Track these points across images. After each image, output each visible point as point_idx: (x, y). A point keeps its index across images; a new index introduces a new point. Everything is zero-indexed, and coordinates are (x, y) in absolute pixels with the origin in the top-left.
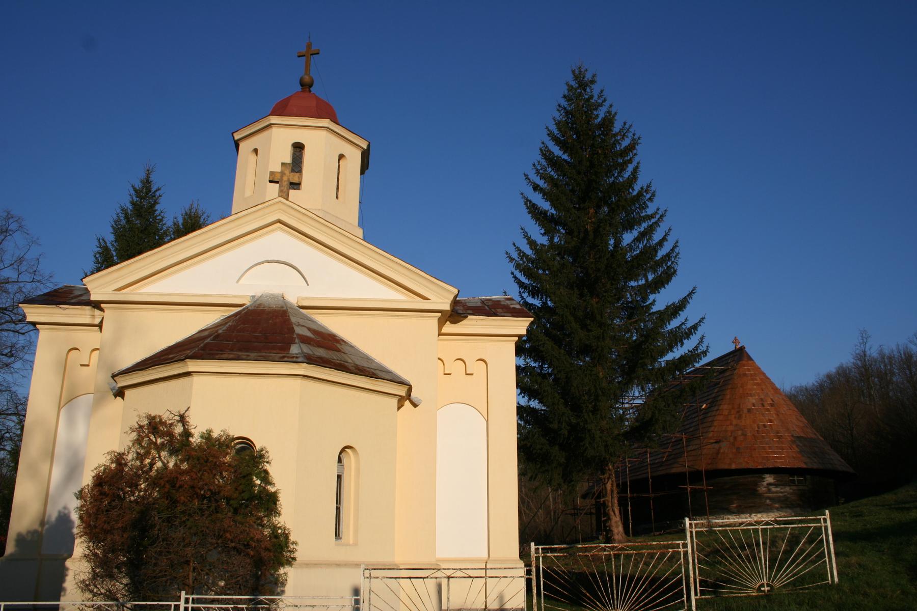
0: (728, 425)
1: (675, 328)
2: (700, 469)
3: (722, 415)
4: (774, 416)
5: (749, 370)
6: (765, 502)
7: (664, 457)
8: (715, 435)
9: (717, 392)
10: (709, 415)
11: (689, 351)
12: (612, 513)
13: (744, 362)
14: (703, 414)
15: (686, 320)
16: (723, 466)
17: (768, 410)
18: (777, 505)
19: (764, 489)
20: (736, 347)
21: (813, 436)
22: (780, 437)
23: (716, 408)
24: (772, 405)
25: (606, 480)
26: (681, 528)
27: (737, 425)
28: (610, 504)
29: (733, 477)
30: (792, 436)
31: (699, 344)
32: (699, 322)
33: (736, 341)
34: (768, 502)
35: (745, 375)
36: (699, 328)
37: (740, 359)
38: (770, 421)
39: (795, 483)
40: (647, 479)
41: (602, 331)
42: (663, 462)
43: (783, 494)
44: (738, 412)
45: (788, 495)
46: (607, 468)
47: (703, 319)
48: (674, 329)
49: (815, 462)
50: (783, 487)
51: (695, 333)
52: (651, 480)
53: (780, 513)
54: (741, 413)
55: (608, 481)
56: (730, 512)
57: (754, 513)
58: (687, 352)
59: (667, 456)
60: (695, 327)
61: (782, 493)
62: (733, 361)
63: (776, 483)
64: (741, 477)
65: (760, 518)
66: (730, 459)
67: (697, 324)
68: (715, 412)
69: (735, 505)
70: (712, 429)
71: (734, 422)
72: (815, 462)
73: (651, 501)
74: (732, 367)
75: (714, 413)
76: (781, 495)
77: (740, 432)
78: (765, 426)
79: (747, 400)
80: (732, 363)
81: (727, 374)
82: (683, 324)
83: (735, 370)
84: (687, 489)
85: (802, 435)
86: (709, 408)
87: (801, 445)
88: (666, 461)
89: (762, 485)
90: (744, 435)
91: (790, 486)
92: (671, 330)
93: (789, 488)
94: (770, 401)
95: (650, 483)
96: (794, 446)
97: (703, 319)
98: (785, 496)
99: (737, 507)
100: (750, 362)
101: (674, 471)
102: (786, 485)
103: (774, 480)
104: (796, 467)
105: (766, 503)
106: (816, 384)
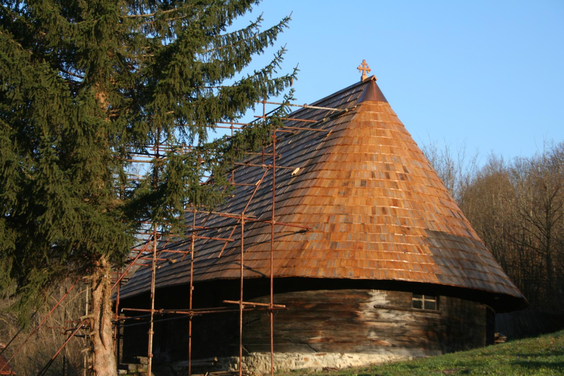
0: (326, 205)
1: (239, 31)
2: (267, 274)
3: (320, 187)
4: (404, 196)
5: (375, 116)
6: (369, 335)
7: (220, 251)
8: (302, 220)
9: (321, 149)
10: (300, 185)
11: (256, 74)
12: (98, 340)
13: (370, 103)
14: (291, 184)
15: (259, 19)
16: (305, 272)
17: (395, 185)
18: (386, 342)
19: (369, 314)
20: (362, 78)
21: (462, 233)
22: (405, 231)
23: (312, 175)
24: (403, 177)
25: (95, 284)
26: (233, 370)
27: (339, 205)
28: (97, 326)
29: (322, 291)
30: (427, 230)
31: (274, 62)
32: (280, 25)
33: (364, 67)
34: (373, 335)
35: (367, 124)
36: (279, 35)
37: (365, 98)
38: (395, 203)
39: (421, 308)
40: (188, 284)
41: (96, 22)
42: (218, 258)
43: (399, 325)
44: (346, 184)
45: (407, 327)
46: (98, 263)
47: (286, 19)
48: (238, 34)
49: (455, 276)
50: (400, 312)
51: (272, 43)
52: (193, 288)
53: (391, 354)
54: (350, 186)
55: (97, 287)
56: (311, 349)
57: (347, 352)
58: (252, 74)
59: (225, 250)
60: (272, 33)
61: (397, 322)
62: (354, 100)
63: (390, 305)
64: (334, 291)
65: (357, 361)
66: (319, 261)
67: (276, 27)
68: (309, 181)
69: (319, 338)
70: (298, 209)
71: (336, 201)
72: (455, 276)
73: (190, 322)
74: (350, 110)
75: (307, 184)
76: (395, 325)
77: (342, 218)
78: (384, 210)
79: (364, 166)
80: (351, 104)
81: (341, 120)
82: (253, 25)
83: (354, 114)
84: (238, 306)
85: (444, 229)
86: (302, 174)
87: (438, 246)
88: (221, 257)
89: (367, 307)
90: (349, 223)
91: (411, 311)
92: (232, 34)
93: (410, 315)
94: (400, 171)
95: (191, 293)
96: (426, 248)
97: (286, 19)
98: (402, 327)
99: (322, 341)
100: (381, 104)
101: (228, 274)
102: (406, 310)
103: (387, 300)
104: (422, 281)
105: (369, 337)
106: (548, 157)
